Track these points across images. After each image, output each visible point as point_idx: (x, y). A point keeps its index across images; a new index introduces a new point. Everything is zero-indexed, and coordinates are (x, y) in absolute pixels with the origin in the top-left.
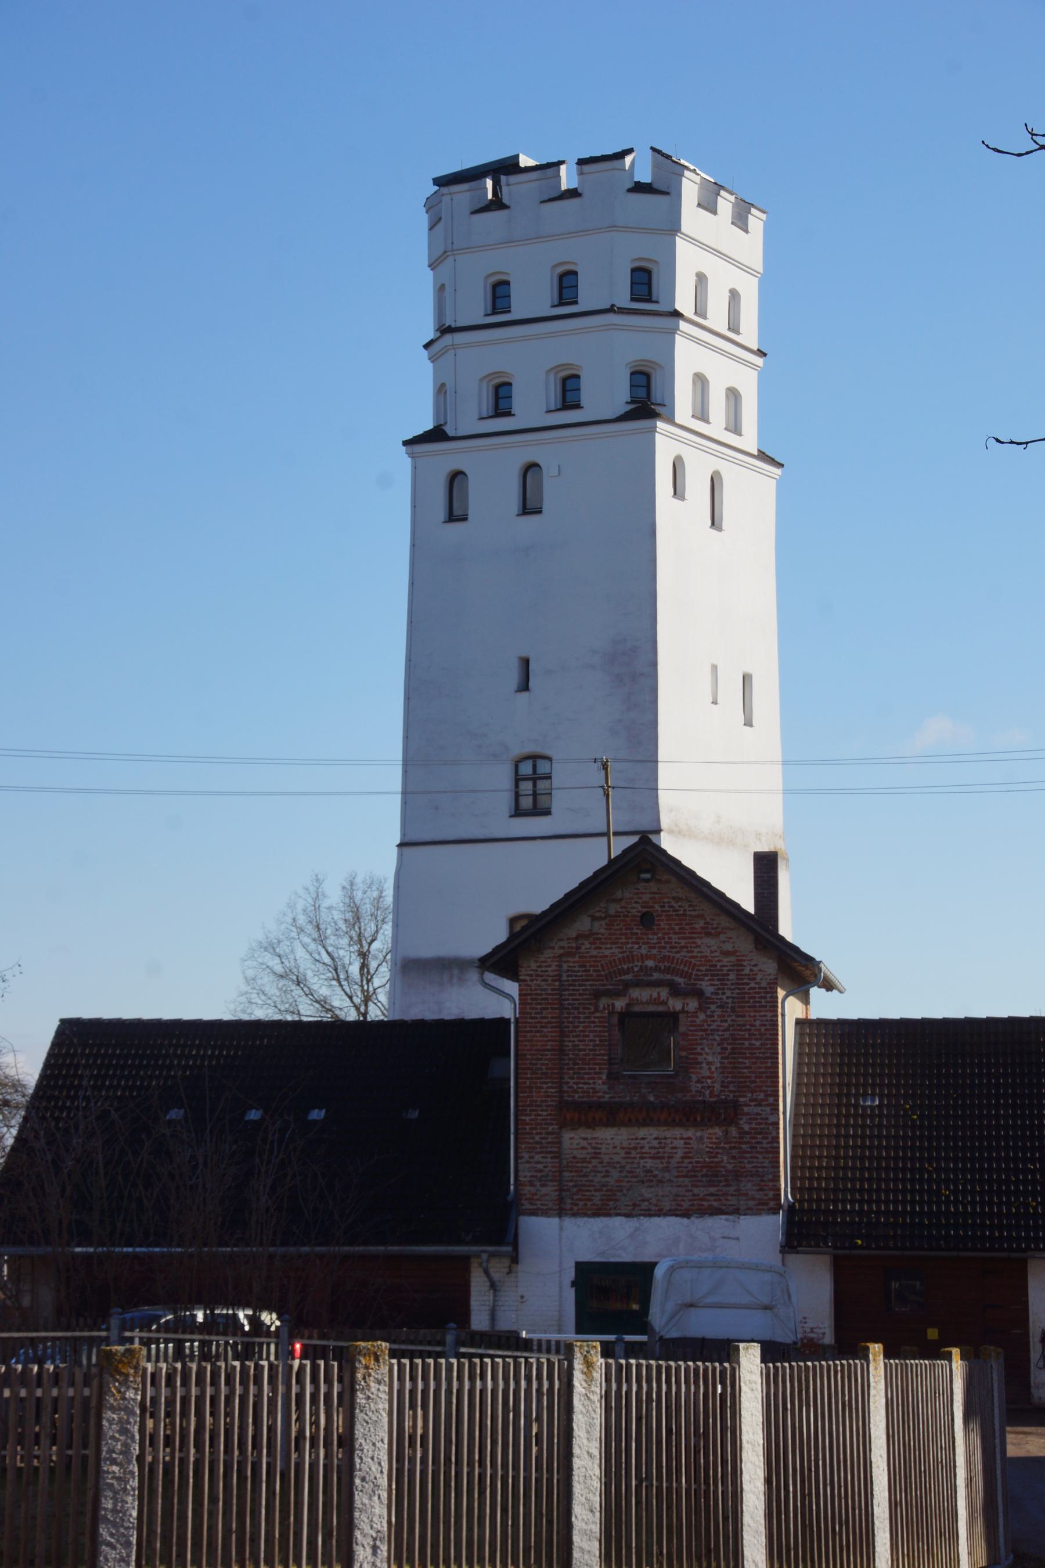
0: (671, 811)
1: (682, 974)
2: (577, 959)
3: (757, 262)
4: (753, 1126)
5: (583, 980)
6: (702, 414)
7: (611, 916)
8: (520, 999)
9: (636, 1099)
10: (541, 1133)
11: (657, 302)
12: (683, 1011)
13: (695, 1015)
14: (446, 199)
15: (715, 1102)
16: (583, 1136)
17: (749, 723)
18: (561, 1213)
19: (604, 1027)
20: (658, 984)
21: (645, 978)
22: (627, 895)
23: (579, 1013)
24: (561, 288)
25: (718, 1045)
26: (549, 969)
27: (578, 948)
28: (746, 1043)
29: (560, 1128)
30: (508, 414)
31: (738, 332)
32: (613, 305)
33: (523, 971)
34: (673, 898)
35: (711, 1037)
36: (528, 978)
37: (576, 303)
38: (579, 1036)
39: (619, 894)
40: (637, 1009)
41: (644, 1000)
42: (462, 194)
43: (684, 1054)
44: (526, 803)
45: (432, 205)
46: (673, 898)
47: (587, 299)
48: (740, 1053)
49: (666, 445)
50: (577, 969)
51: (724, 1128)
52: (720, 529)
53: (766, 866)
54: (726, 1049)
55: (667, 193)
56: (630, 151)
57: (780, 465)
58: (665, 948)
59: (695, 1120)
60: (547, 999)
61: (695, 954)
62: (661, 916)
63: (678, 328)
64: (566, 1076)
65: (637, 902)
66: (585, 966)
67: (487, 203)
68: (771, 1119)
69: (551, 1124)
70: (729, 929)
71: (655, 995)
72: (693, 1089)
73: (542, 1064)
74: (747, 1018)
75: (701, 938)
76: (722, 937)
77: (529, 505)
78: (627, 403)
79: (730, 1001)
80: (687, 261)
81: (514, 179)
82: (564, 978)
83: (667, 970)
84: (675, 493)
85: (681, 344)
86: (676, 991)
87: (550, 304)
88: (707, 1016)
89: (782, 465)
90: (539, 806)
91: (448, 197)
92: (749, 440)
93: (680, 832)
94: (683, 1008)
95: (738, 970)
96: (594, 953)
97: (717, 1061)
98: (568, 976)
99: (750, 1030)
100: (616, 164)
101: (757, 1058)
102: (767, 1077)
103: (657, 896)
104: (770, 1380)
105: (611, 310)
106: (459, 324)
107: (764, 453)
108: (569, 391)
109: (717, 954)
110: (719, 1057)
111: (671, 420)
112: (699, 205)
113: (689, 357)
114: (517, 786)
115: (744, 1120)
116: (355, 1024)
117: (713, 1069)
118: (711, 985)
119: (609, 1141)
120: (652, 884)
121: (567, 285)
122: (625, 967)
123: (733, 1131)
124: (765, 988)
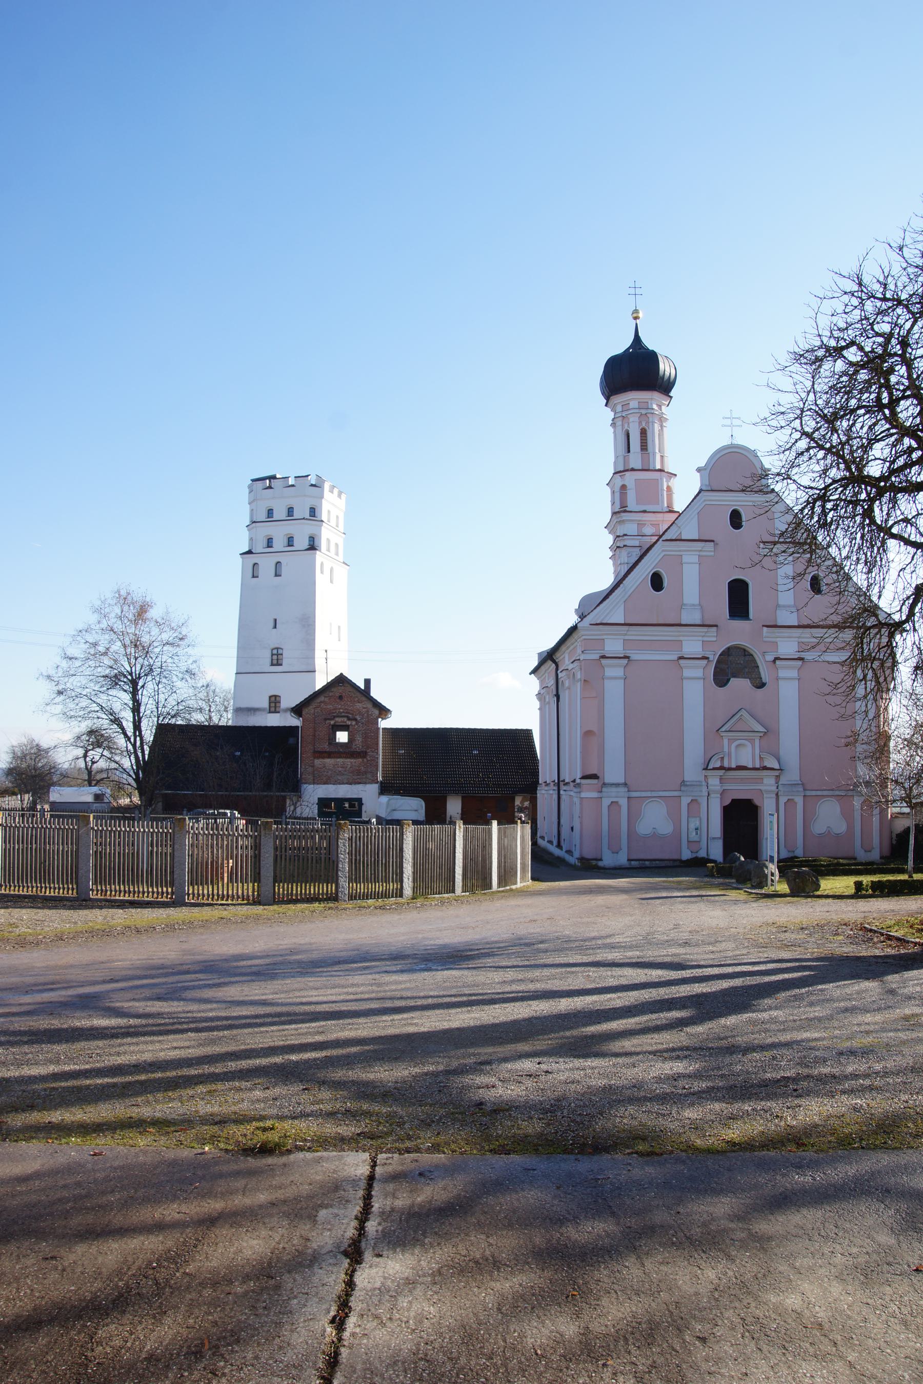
6: (328, 550)
18: (314, 783)
33: (304, 713)
44: (275, 662)
45: (250, 487)
47: (276, 516)
53: (367, 682)
86: (349, 719)
92: (341, 558)
104: (499, 830)
108: (290, 541)
121: (290, 511)
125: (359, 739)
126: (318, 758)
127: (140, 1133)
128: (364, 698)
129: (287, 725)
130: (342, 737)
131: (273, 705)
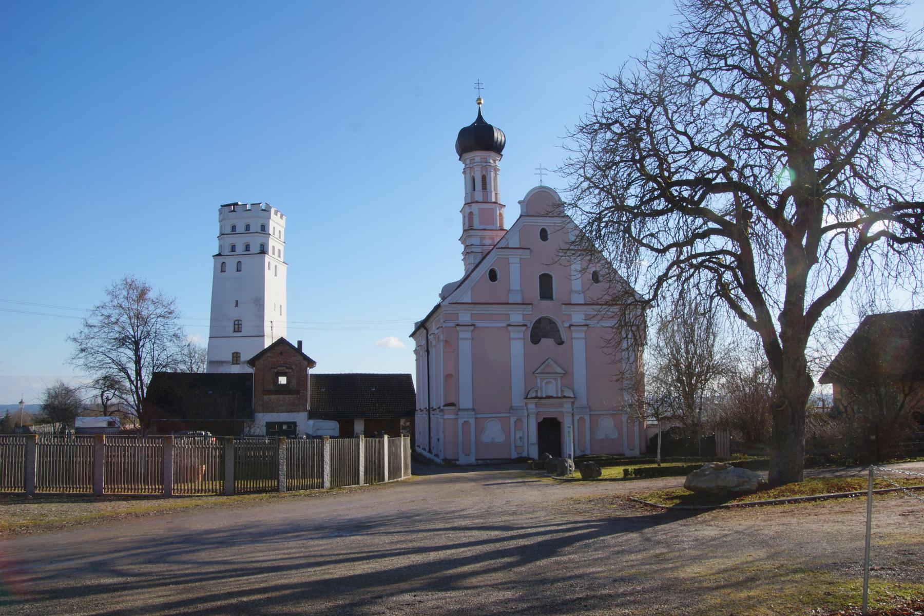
42: (227, 209)
49: (267, 259)
53: (300, 343)
85: (270, 240)
92: (282, 259)
104: (389, 441)
108: (247, 248)
121: (248, 227)
125: (294, 381)
129: (245, 372)
130: (283, 380)
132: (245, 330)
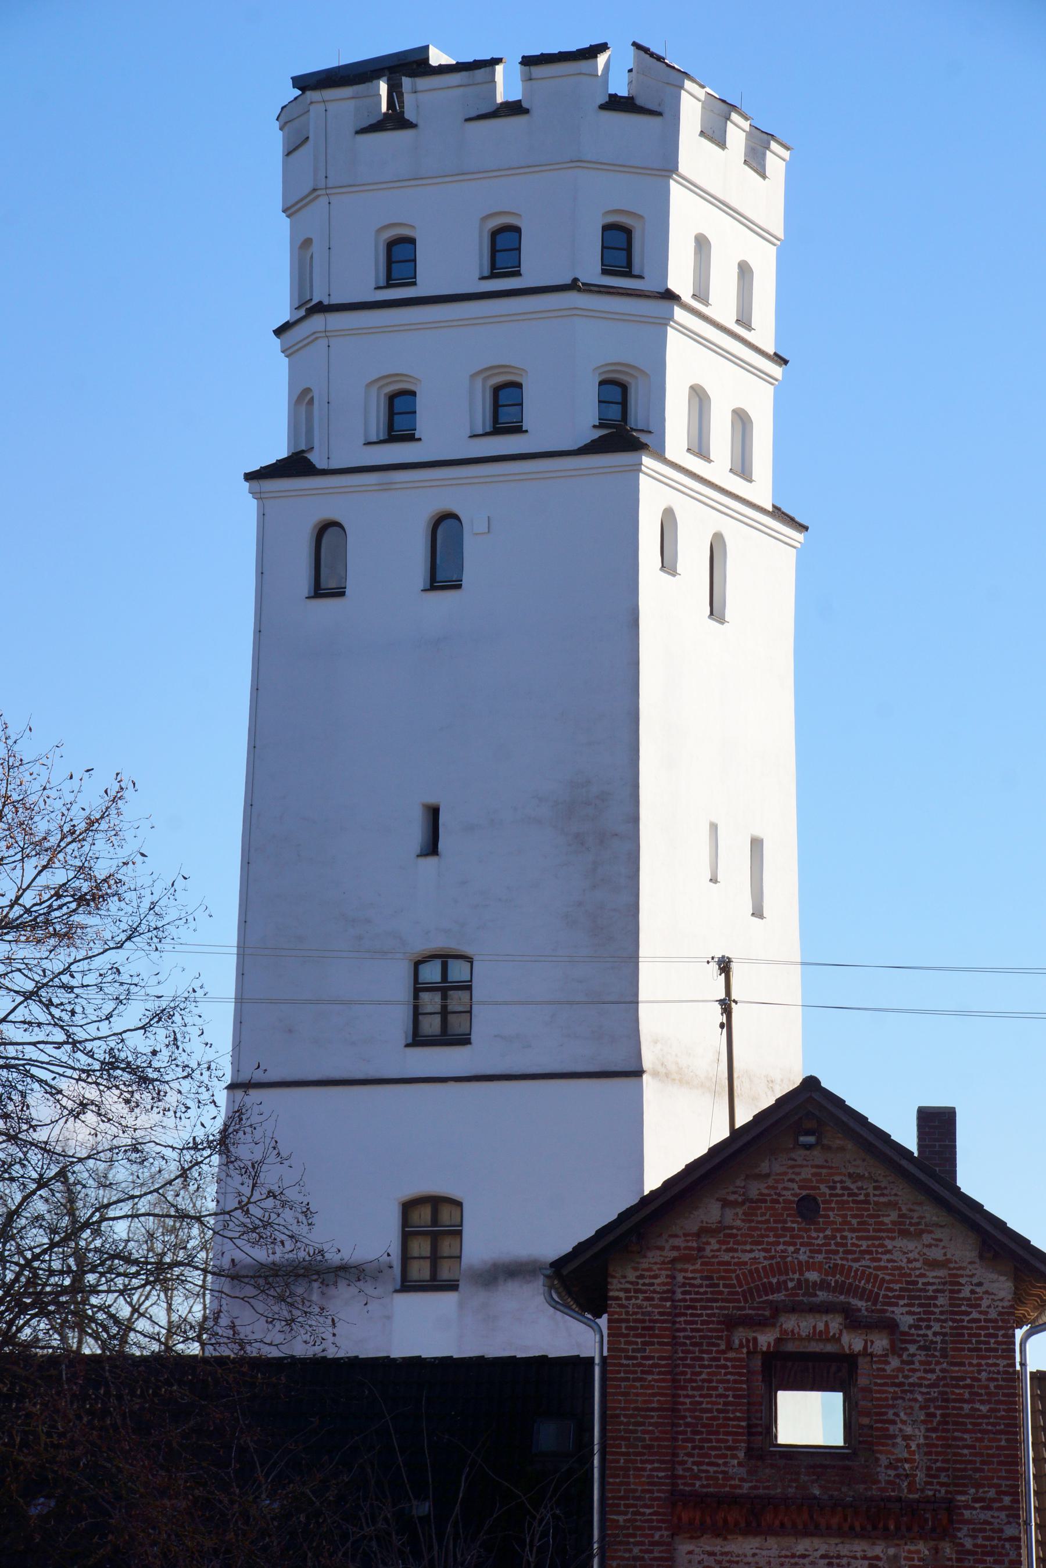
0: (656, 1042)
1: (862, 1294)
2: (698, 1266)
3: (775, 222)
4: (979, 1541)
5: (709, 1300)
6: (700, 449)
7: (752, 1201)
8: (609, 1328)
9: (791, 1491)
10: (642, 1543)
11: (640, 277)
12: (865, 1353)
13: (884, 1359)
14: (316, 110)
15: (918, 1501)
16: (708, 1548)
17: (758, 913)
19: (741, 1374)
20: (825, 1309)
21: (805, 1299)
22: (777, 1168)
23: (702, 1352)
24: (494, 251)
25: (921, 1408)
26: (656, 1281)
27: (700, 1249)
28: (966, 1407)
29: (673, 1535)
30: (410, 437)
31: (749, 327)
32: (575, 280)
33: (616, 1289)
34: (850, 1175)
35: (909, 1396)
36: (622, 1294)
37: (518, 274)
38: (701, 1388)
39: (764, 1167)
40: (790, 1347)
41: (804, 1334)
43: (865, 1421)
44: (431, 1025)
45: (288, 117)
46: (850, 1175)
48: (956, 1423)
49: (654, 491)
50: (698, 1282)
51: (932, 1543)
52: (721, 620)
53: (937, 1125)
54: (934, 1415)
55: (659, 114)
56: (603, 47)
57: (803, 528)
58: (836, 1252)
59: (886, 1528)
60: (652, 1328)
61: (882, 1264)
62: (830, 1202)
63: (671, 317)
64: (681, 1452)
65: (792, 1180)
66: (711, 1278)
67: (381, 117)
68: (1009, 1531)
69: (659, 1529)
70: (937, 1225)
71: (821, 1326)
72: (882, 1478)
73: (644, 1432)
74: (967, 1368)
75: (893, 1239)
76: (927, 1239)
77: (440, 576)
78: (595, 426)
79: (939, 1339)
80: (686, 216)
81: (423, 83)
82: (679, 1296)
83: (840, 1288)
84: (663, 566)
86: (853, 1322)
87: (477, 276)
88: (903, 1362)
89: (806, 528)
90: (450, 1031)
91: (321, 107)
93: (667, 1075)
94: (865, 1347)
95: (952, 1291)
96: (726, 1257)
97: (919, 1434)
98: (684, 1293)
99: (971, 1386)
100: (583, 65)
101: (987, 1432)
102: (1000, 1463)
103: (824, 1171)
105: (574, 286)
106: (336, 300)
107: (779, 509)
108: (504, 406)
109: (918, 1265)
110: (923, 1428)
111: (660, 455)
112: (702, 133)
113: (687, 363)
114: (416, 997)
115: (965, 1531)
116: (155, 1357)
117: (914, 1447)
118: (909, 1313)
119: (750, 1559)
120: (816, 1152)
121: (503, 247)
122: (774, 1281)
123: (948, 1549)
124: (996, 1321)
125: (910, 1432)
126: (696, 1531)
127: (321, 1252)
128: (930, 1213)
129: (496, 1347)
130: (808, 1418)
131: (421, 1247)
132: (497, 1030)
